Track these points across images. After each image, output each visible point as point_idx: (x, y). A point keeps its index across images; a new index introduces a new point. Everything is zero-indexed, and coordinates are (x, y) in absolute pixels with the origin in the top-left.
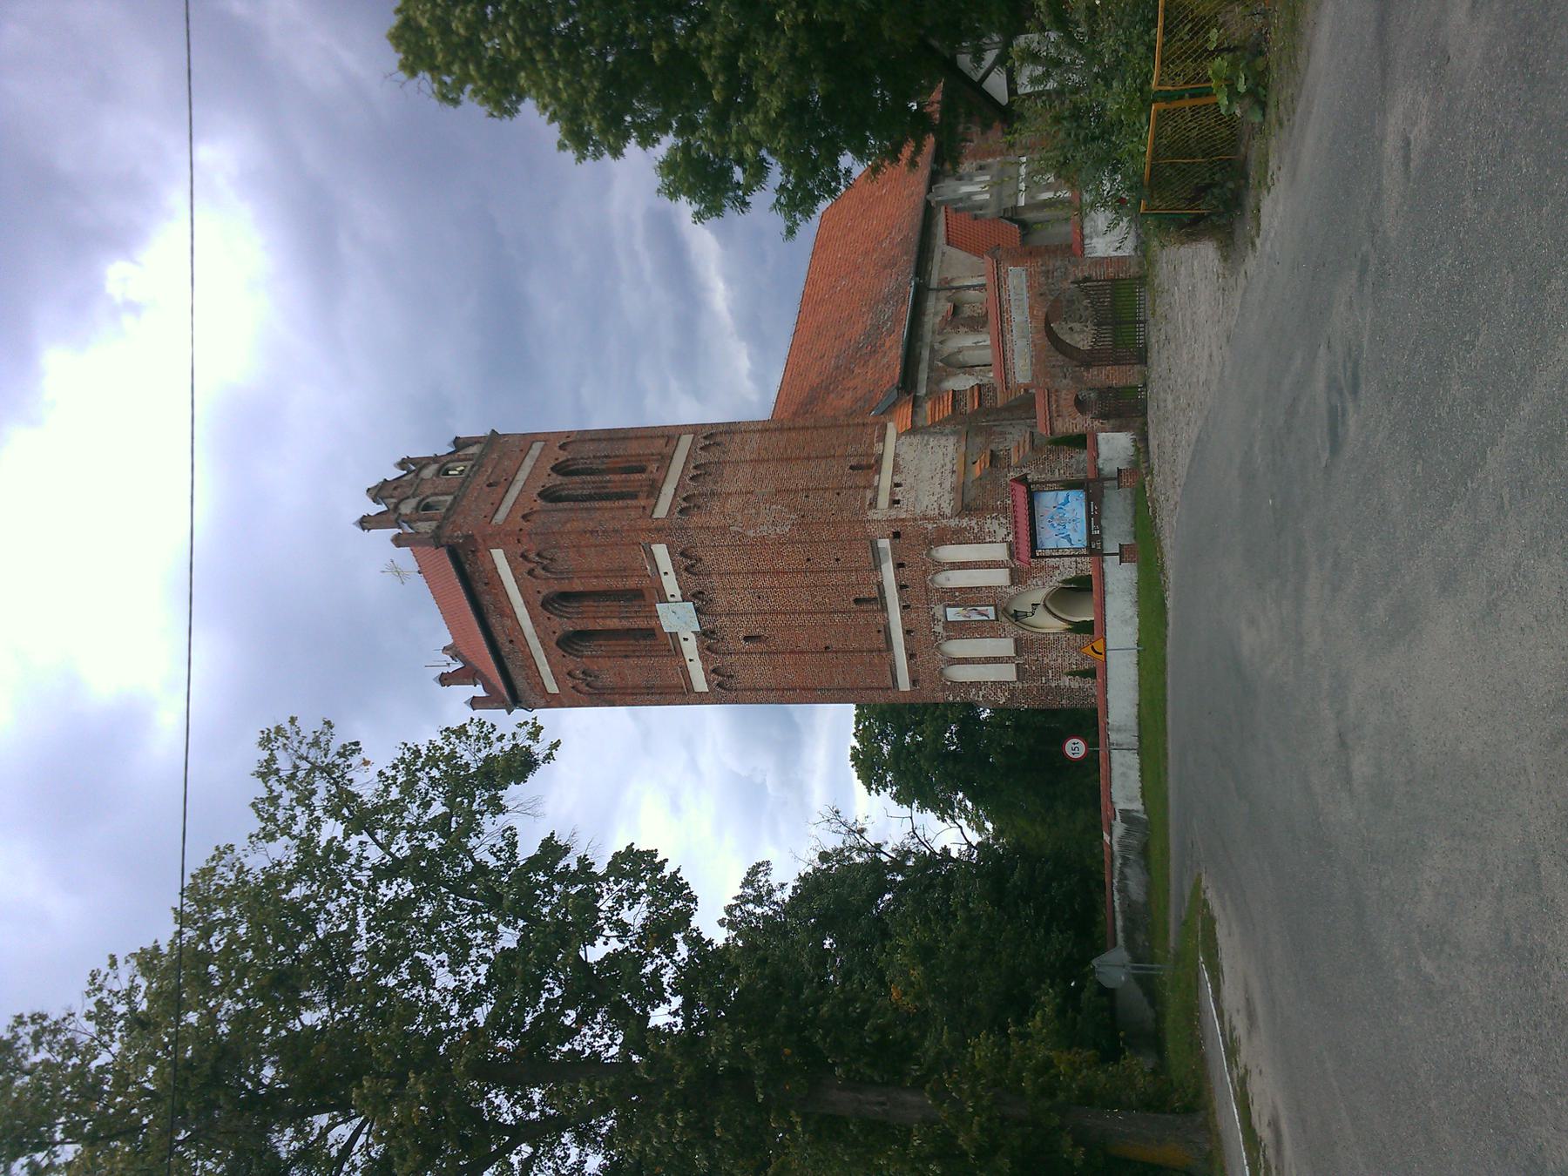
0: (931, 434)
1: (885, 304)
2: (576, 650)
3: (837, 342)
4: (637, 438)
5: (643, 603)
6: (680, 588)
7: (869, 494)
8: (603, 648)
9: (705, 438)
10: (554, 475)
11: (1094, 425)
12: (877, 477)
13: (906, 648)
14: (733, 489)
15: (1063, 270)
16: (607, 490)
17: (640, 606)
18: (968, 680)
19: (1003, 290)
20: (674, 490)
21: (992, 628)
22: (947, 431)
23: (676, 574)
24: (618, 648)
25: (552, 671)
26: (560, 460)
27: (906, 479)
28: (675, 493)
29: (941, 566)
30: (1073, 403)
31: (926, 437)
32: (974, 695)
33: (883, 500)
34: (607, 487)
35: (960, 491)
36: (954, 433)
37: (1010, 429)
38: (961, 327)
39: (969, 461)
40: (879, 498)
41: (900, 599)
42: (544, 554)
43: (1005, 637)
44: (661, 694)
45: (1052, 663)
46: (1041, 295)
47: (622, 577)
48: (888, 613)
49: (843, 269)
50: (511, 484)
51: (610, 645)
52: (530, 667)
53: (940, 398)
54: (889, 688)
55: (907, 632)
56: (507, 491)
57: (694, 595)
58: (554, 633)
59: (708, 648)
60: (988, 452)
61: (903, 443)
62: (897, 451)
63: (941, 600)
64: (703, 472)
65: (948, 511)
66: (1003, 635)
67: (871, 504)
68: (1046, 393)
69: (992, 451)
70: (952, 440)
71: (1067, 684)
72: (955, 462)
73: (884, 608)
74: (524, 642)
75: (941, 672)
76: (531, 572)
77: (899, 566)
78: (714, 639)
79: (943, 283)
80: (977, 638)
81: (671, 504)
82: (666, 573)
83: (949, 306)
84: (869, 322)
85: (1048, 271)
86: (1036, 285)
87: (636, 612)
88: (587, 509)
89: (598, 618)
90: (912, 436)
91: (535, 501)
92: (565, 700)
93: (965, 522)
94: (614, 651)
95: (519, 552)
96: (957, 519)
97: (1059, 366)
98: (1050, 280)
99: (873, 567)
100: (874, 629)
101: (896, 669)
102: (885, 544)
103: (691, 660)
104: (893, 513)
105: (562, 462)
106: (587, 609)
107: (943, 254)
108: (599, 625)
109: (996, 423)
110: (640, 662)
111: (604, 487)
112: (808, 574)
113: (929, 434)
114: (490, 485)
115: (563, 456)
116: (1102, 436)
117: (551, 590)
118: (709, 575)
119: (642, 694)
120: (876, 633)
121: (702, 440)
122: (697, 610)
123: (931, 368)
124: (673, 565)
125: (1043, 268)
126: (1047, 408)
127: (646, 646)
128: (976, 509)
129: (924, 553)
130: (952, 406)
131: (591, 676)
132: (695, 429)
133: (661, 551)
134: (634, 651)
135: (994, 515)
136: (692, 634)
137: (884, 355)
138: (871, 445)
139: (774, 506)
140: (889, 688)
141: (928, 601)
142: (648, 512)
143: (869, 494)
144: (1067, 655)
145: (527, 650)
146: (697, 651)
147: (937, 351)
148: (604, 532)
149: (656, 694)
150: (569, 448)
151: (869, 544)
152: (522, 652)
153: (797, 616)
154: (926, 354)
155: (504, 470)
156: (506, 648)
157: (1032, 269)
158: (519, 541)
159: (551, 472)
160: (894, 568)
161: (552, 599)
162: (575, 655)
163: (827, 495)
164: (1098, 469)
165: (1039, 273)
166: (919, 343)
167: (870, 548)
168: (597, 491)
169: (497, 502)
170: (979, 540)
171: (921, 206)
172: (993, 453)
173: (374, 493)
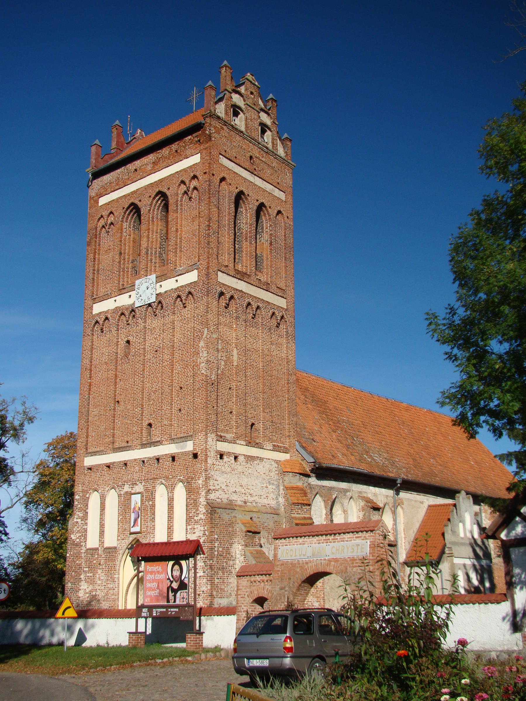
3: (360, 423)
5: (157, 266)
6: (166, 292)
10: (257, 204)
11: (243, 613)
12: (244, 443)
13: (114, 463)
17: (155, 263)
21: (125, 530)
23: (176, 289)
27: (241, 465)
28: (237, 290)
29: (171, 489)
30: (261, 595)
33: (223, 447)
38: (364, 513)
39: (254, 515)
41: (150, 459)
43: (118, 540)
44: (93, 279)
45: (98, 576)
47: (176, 248)
49: (416, 431)
50: (252, 173)
52: (117, 184)
57: (160, 302)
58: (140, 201)
59: (123, 314)
61: (271, 465)
62: (265, 460)
63: (147, 490)
65: (212, 496)
66: (119, 538)
67: (221, 437)
71: (81, 588)
72: (254, 504)
73: (144, 446)
74: (135, 179)
75: (96, 490)
76: (183, 182)
79: (399, 501)
81: (229, 287)
83: (381, 505)
87: (151, 260)
91: (237, 188)
93: (202, 509)
94: (125, 244)
95: (197, 174)
96: (205, 503)
100: (129, 439)
102: (189, 446)
104: (212, 454)
107: (422, 503)
114: (251, 157)
116: (233, 618)
117: (169, 197)
120: (126, 439)
121: (281, 314)
122: (150, 305)
123: (331, 489)
124: (182, 287)
127: (128, 268)
129: (182, 478)
133: (192, 277)
135: (206, 532)
136: (132, 302)
138: (270, 440)
139: (223, 363)
141: (147, 480)
142: (223, 269)
143: (229, 436)
144: (103, 588)
147: (345, 495)
148: (208, 234)
149: (94, 276)
153: (141, 379)
155: (263, 169)
156: (131, 167)
158: (205, 173)
159: (259, 202)
160: (172, 454)
162: (124, 216)
167: (185, 435)
170: (189, 520)
171: (455, 487)
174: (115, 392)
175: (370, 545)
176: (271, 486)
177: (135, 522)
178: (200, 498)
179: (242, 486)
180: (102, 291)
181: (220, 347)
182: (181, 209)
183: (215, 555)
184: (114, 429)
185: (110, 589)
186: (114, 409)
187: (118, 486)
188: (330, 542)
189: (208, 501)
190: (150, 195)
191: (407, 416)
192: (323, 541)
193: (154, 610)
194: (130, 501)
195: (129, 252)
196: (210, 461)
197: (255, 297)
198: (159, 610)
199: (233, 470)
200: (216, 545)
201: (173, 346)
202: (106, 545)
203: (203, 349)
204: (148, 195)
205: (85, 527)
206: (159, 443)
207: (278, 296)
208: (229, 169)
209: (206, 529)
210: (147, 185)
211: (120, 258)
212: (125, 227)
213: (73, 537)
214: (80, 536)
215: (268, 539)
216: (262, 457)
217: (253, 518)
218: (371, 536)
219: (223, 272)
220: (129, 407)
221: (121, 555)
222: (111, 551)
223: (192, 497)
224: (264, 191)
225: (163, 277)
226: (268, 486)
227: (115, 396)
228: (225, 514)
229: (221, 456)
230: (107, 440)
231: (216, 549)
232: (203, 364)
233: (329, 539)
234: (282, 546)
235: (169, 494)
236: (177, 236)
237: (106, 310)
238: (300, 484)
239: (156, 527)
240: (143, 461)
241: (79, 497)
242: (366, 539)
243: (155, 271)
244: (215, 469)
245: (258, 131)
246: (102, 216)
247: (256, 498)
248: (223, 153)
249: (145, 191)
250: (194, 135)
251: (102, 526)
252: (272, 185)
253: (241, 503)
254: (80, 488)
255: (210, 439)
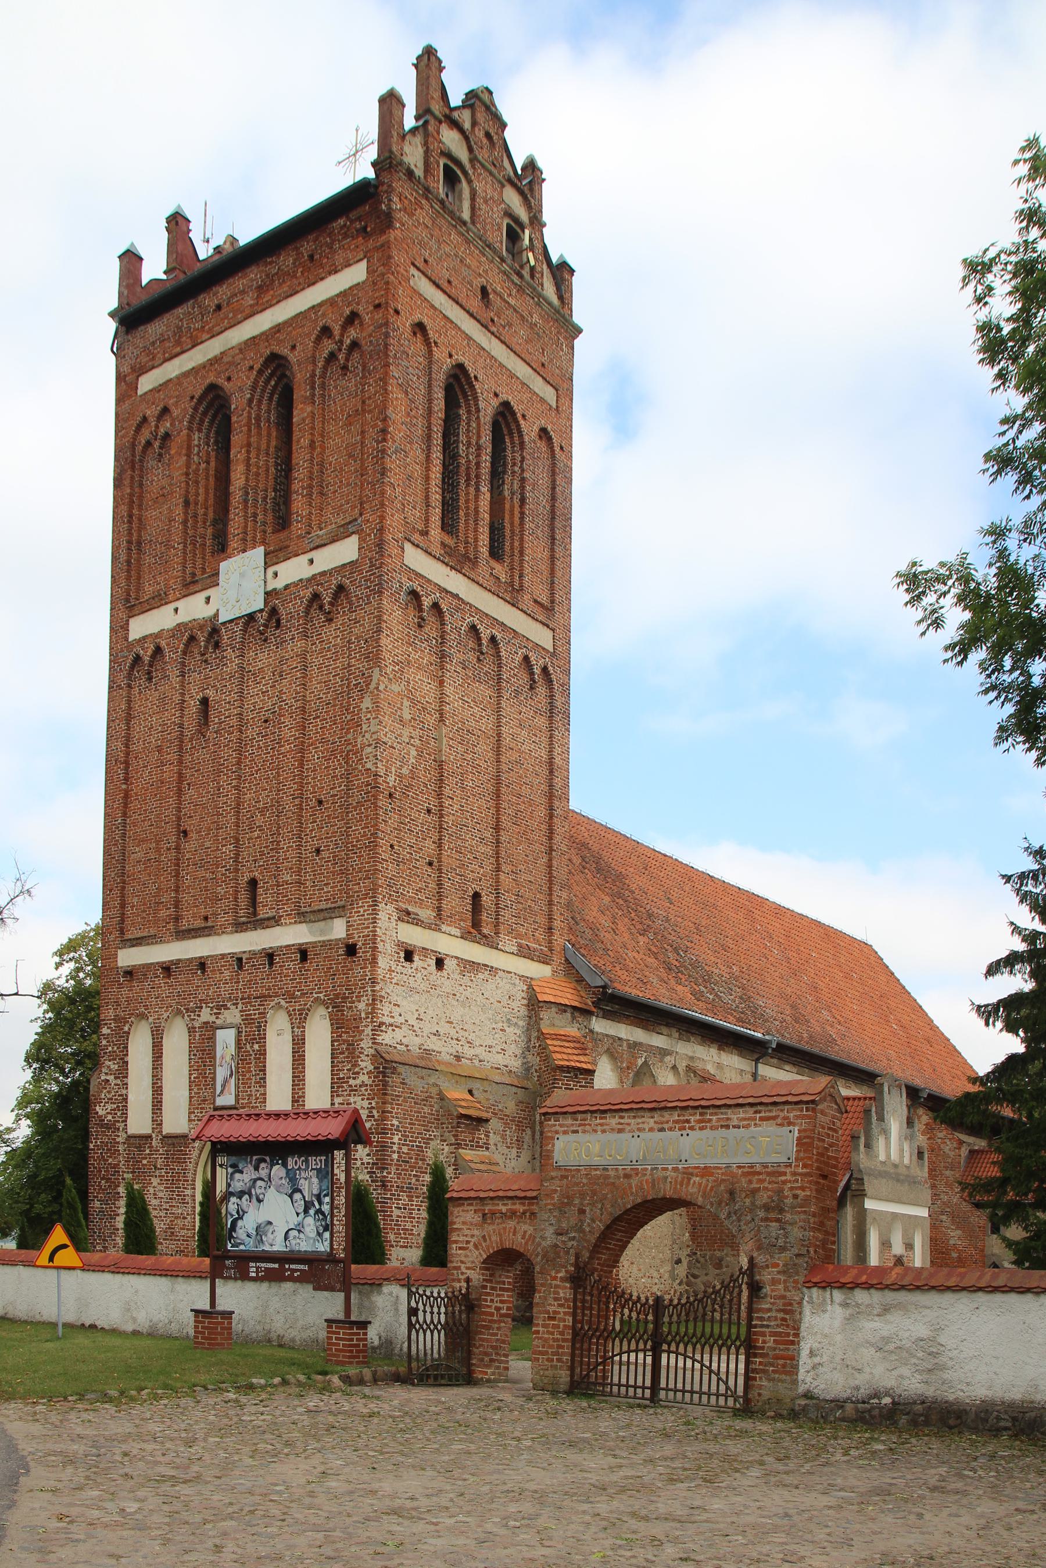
0: (528, 1030)
1: (741, 998)
2: (202, 421)
3: (692, 925)
4: (552, 558)
6: (287, 587)
7: (426, 914)
8: (203, 466)
9: (545, 669)
10: (495, 403)
12: (458, 932)
13: (179, 960)
14: (449, 690)
15: (780, 1242)
16: (463, 486)
17: (264, 523)
18: (130, 1059)
19: (750, 1112)
20: (455, 592)
22: (530, 1057)
23: (309, 580)
24: (201, 491)
25: (170, 381)
26: (522, 422)
28: (447, 592)
29: (299, 1019)
31: (521, 1023)
32: (109, 1067)
34: (468, 485)
35: (422, 1063)
36: (527, 1068)
37: (525, 1155)
39: (476, 1086)
40: (419, 929)
41: (253, 954)
42: (356, 355)
43: (190, 1120)
44: (128, 562)
45: (152, 1190)
46: (732, 1193)
47: (310, 487)
48: (232, 933)
50: (485, 327)
51: (207, 479)
52: (178, 343)
53: (583, 1050)
54: (122, 933)
55: (202, 964)
56: (472, 315)
57: (274, 612)
58: (229, 379)
59: (192, 639)
60: (484, 1115)
62: (500, 973)
63: (248, 1020)
64: (485, 650)
65: (387, 1038)
67: (408, 913)
68: (529, 1194)
69: (487, 1121)
70: (515, 1064)
72: (476, 1062)
73: (240, 927)
74: (217, 329)
75: (142, 1016)
76: (326, 331)
77: (304, 953)
78: (206, 647)
80: (190, 1074)
81: (429, 581)
82: (311, 561)
84: (717, 971)
85: (781, 1211)
86: (755, 1185)
87: (255, 515)
88: (429, 437)
89: (248, 452)
90: (525, 1002)
92: (127, 405)
93: (366, 1064)
94: (197, 482)
97: (582, 1221)
98: (761, 1214)
99: (303, 909)
100: (210, 911)
101: (148, 944)
102: (338, 929)
103: (176, 610)
105: (518, 426)
106: (264, 433)
108: (237, 453)
109: (538, 1134)
110: (177, 526)
111: (468, 480)
112: (297, 801)
113: (528, 1030)
114: (484, 291)
115: (530, 430)
117: (296, 368)
118: (305, 635)
119: (130, 534)
120: (203, 912)
121: (541, 662)
122: (251, 617)
123: (634, 1046)
124: (323, 574)
125: (789, 1201)
126: (501, 1194)
127: (203, 537)
128: (385, 1084)
130: (568, 1067)
131: (160, 448)
132: (561, 652)
133: (346, 551)
134: (195, 516)
135: (375, 1112)
137: (662, 980)
139: (414, 753)
140: (122, 933)
141: (247, 1000)
142: (416, 537)
144: (162, 1214)
145: (205, 336)
146: (190, 619)
149: (129, 555)
150: (542, 445)
151: (340, 903)
152: (202, 327)
153: (234, 783)
154: (658, 1041)
155: (510, 325)
156: (208, 300)
157: (788, 1177)
160: (300, 944)
161: (283, 375)
162: (192, 417)
163: (428, 843)
164: (380, 1285)
165: (780, 1191)
166: (677, 1035)
167: (330, 905)
168: (463, 468)
169: (453, 292)
172: (481, 1121)
173: (485, 97)
174: (179, 810)
175: (798, 1139)
176: (511, 1029)
177: (224, 1086)
178: (362, 1040)
179: (451, 1023)
180: (149, 589)
181: (407, 716)
182: (323, 396)
183: (392, 1160)
184: (177, 891)
185: (176, 1218)
186: (178, 848)
187: (187, 1010)
188: (692, 1128)
189: (379, 1048)
190: (251, 363)
191: (777, 925)
192: (670, 1124)
193: (252, 1264)
194: (214, 1043)
195: (206, 500)
196: (383, 962)
197: (487, 615)
198: (263, 1265)
199: (434, 987)
200: (396, 1139)
201: (303, 710)
202: (167, 1129)
203: (369, 716)
204: (247, 364)
205: (124, 1092)
206: (273, 922)
207: (537, 620)
208: (433, 306)
209: (373, 1105)
210: (246, 342)
211: (186, 513)
212: (196, 442)
213: (100, 1110)
214: (114, 1110)
215: (504, 1137)
216: (495, 966)
217: (475, 1092)
218: (803, 1117)
219: (417, 546)
220: (207, 844)
221: (196, 1153)
222: (177, 1142)
223: (345, 1036)
224: (512, 376)
225: (281, 555)
226: (507, 1029)
227: (179, 818)
228: (415, 1078)
229: (409, 956)
230: (163, 913)
231: (395, 1148)
232: (369, 750)
233: (688, 1121)
234: (565, 1133)
235: (295, 1029)
236: (312, 459)
237: (156, 631)
238: (573, 1031)
239: (267, 1096)
240: (240, 960)
241: (109, 1031)
242: (790, 1124)
243: (263, 543)
244: (394, 981)
245: (500, 229)
246: (145, 419)
247: (479, 1051)
248: (420, 264)
249: (241, 356)
250: (353, 215)
251: (157, 1090)
252: (528, 364)
253: (445, 1057)
254: (111, 1014)
255: (382, 916)
